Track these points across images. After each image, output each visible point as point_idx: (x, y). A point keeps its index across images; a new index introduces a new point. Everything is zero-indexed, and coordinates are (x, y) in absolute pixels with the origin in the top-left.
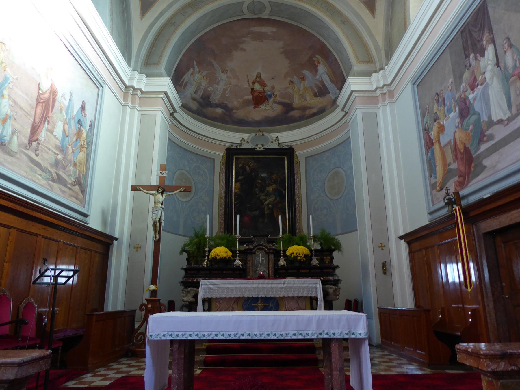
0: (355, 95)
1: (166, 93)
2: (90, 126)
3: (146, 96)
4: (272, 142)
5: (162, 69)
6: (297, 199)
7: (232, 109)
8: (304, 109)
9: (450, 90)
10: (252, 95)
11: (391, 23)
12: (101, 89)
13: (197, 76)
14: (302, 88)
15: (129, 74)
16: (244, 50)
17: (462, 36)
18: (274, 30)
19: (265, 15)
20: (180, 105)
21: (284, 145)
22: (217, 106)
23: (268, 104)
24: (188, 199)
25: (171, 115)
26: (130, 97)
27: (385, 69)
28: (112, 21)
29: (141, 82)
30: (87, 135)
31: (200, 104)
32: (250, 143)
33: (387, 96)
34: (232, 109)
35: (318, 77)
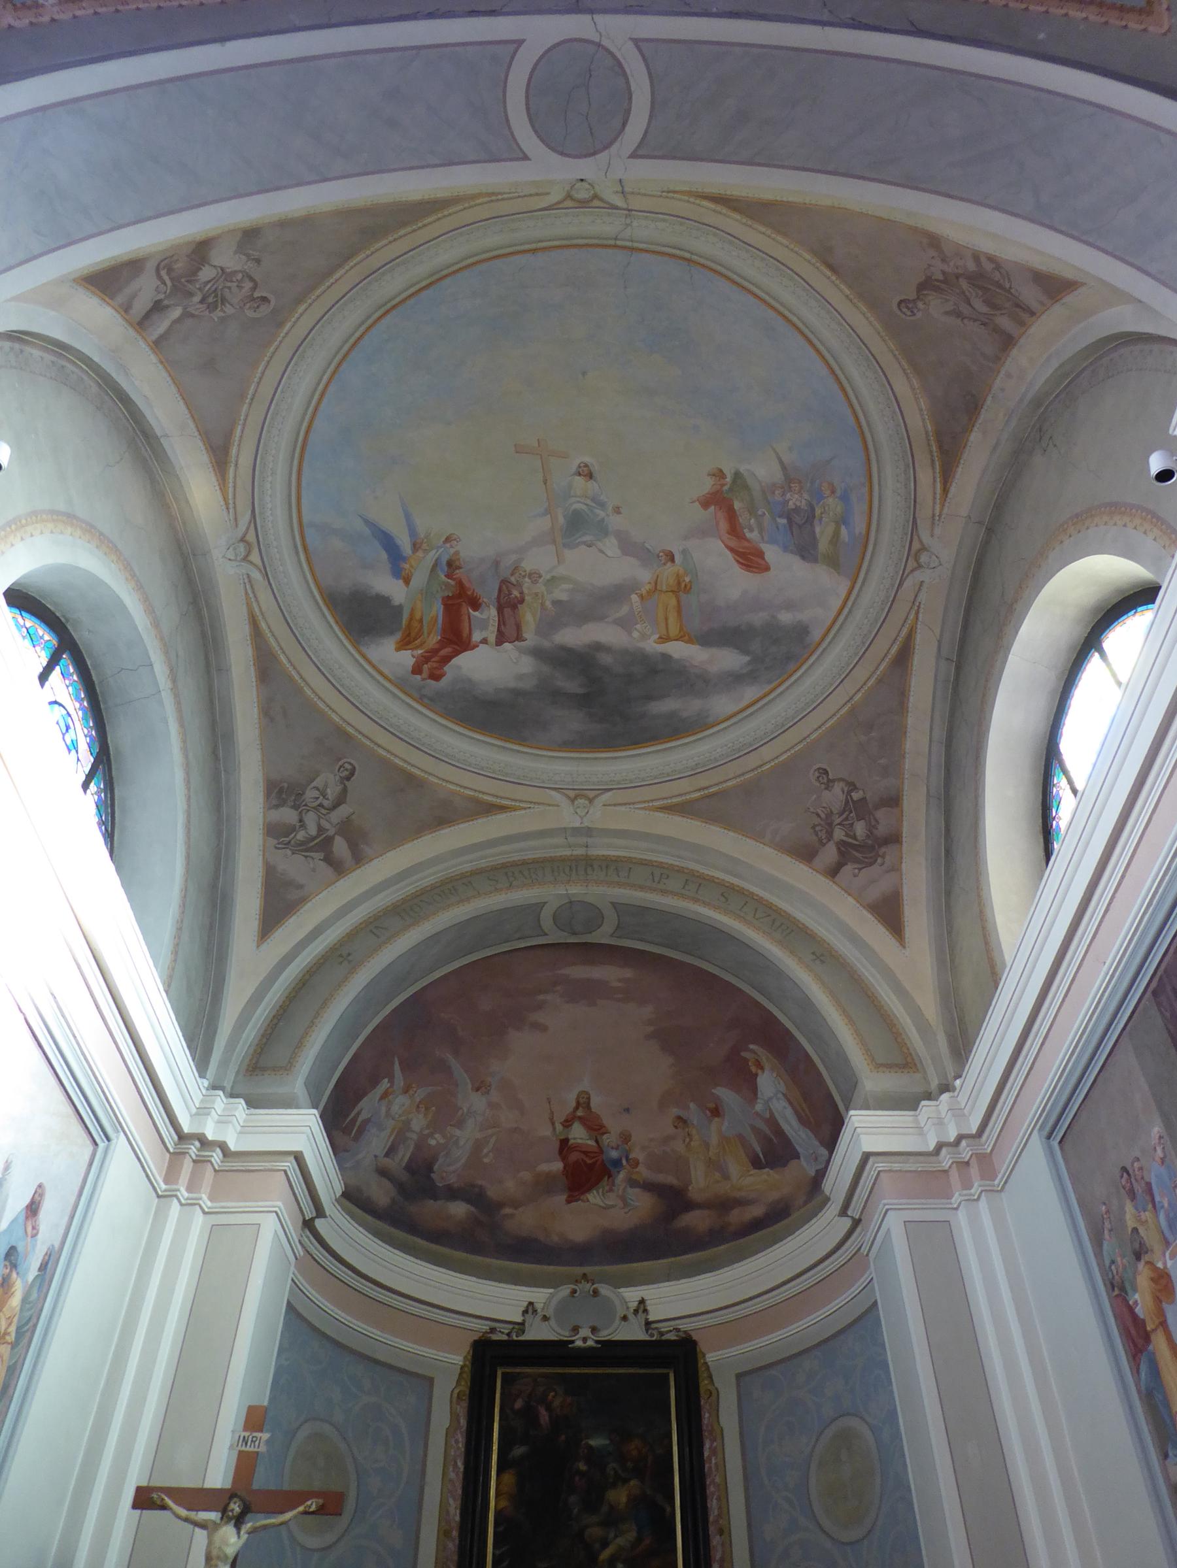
0: (874, 1166)
1: (298, 1158)
2: (43, 1267)
3: (237, 1165)
4: (625, 1318)
5: (298, 1084)
6: (715, 1541)
7: (501, 1205)
8: (724, 1205)
9: (1163, 1160)
10: (564, 1158)
11: (952, 961)
12: (102, 1145)
13: (400, 1103)
14: (714, 1140)
15: (197, 1098)
16: (544, 1028)
17: (1159, 1004)
18: (628, 973)
19: (602, 936)
20: (339, 1193)
21: (664, 1327)
22: (453, 1194)
23: (611, 1190)
24: (329, 1538)
25: (308, 1224)
26: (187, 1166)
27: (954, 1089)
28: (175, 953)
29: (230, 1123)
30: (24, 1300)
31: (401, 1187)
32: (553, 1322)
33: (974, 1171)
34: (501, 1205)
35: (759, 1107)
